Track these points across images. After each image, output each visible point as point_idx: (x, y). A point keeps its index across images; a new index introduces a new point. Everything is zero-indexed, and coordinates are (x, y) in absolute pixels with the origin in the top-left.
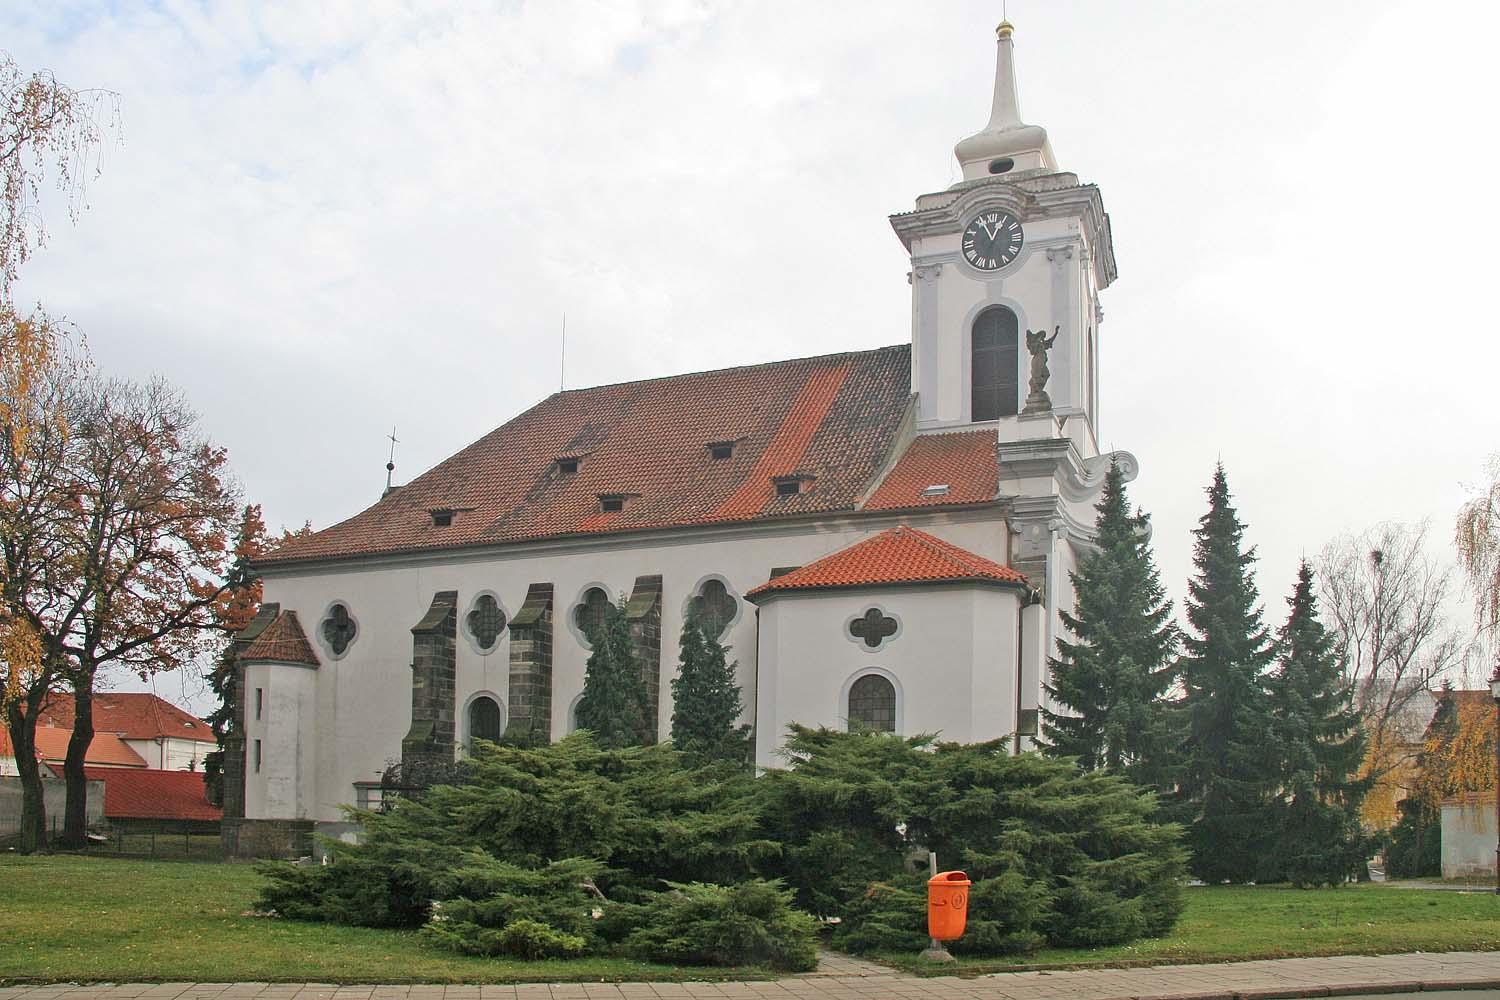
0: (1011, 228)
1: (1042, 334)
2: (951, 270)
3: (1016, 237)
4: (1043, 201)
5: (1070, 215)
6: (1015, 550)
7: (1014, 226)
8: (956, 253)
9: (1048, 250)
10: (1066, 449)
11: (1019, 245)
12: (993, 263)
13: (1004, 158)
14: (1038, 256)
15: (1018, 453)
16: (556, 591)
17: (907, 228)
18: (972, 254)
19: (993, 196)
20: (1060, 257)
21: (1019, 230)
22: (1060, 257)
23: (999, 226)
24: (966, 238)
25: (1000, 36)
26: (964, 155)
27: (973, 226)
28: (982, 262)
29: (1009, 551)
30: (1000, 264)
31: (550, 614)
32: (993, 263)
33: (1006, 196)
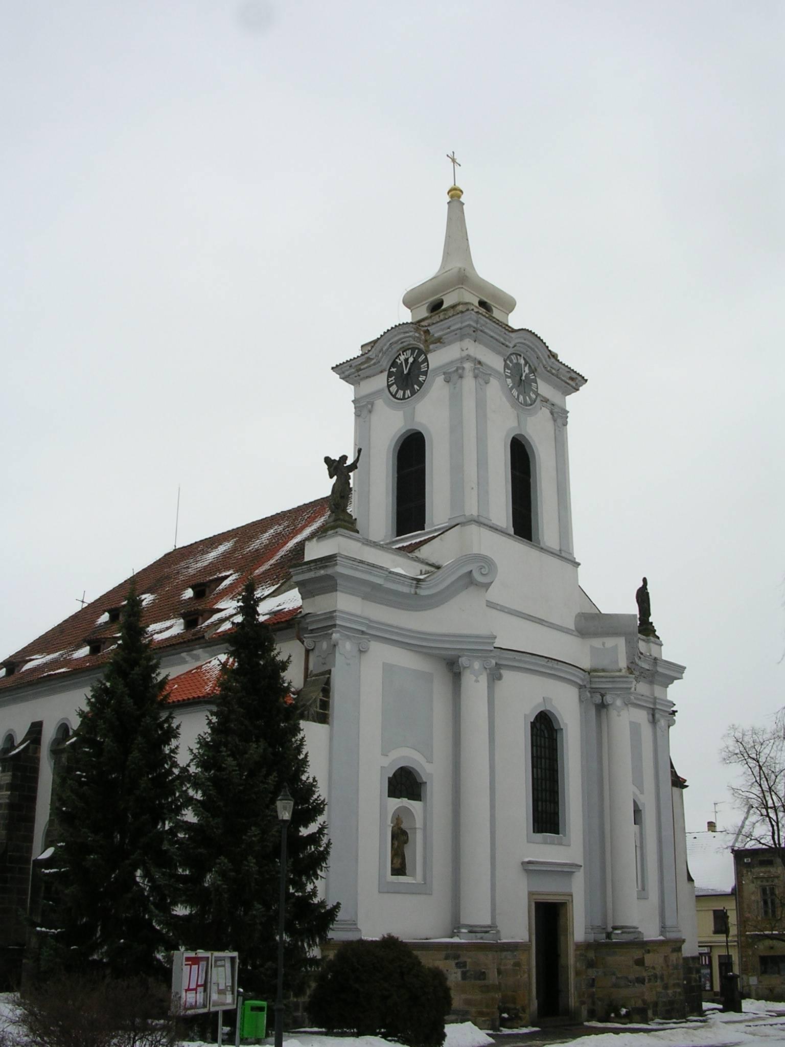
0: (420, 360)
1: (344, 458)
2: (380, 404)
3: (423, 367)
4: (437, 331)
5: (461, 339)
6: (311, 667)
7: (423, 357)
8: (382, 390)
9: (444, 373)
10: (336, 564)
11: (425, 373)
12: (408, 392)
13: (436, 300)
14: (440, 380)
15: (303, 572)
16: (44, 725)
17: (349, 371)
18: (394, 389)
19: (402, 336)
20: (455, 377)
21: (426, 360)
22: (455, 377)
23: (411, 360)
24: (389, 376)
25: (452, 197)
26: (410, 302)
27: (394, 364)
28: (401, 393)
29: (306, 668)
30: (413, 393)
31: (36, 748)
32: (408, 392)
33: (411, 334)
